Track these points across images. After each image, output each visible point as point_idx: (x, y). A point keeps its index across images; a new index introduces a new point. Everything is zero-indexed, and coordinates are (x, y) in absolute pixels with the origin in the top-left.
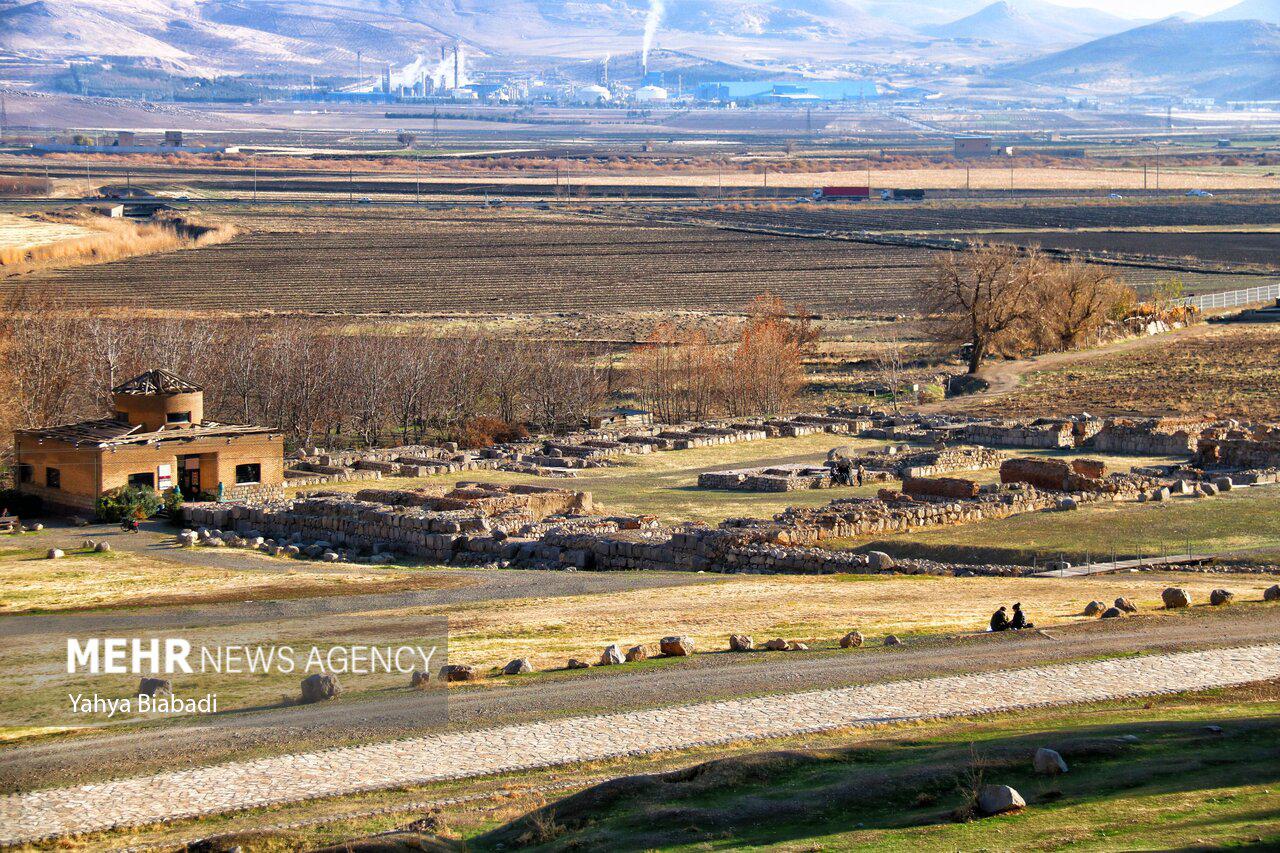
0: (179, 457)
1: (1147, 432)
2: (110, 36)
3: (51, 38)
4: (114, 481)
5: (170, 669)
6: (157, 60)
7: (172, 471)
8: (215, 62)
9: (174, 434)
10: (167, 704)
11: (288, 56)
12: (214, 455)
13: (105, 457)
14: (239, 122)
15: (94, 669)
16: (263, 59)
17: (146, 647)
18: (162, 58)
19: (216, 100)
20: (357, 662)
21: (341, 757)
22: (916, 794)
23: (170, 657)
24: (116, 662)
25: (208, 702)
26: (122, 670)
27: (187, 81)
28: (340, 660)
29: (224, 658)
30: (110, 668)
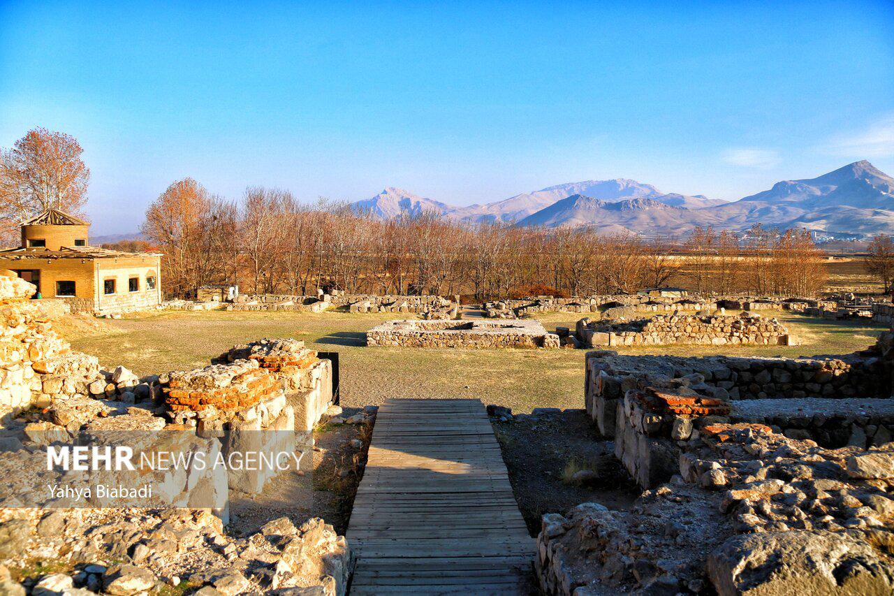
5: (118, 468)
10: (116, 492)
20: (162, 462)
21: (867, 402)
22: (824, 515)
28: (237, 461)
29: (156, 460)
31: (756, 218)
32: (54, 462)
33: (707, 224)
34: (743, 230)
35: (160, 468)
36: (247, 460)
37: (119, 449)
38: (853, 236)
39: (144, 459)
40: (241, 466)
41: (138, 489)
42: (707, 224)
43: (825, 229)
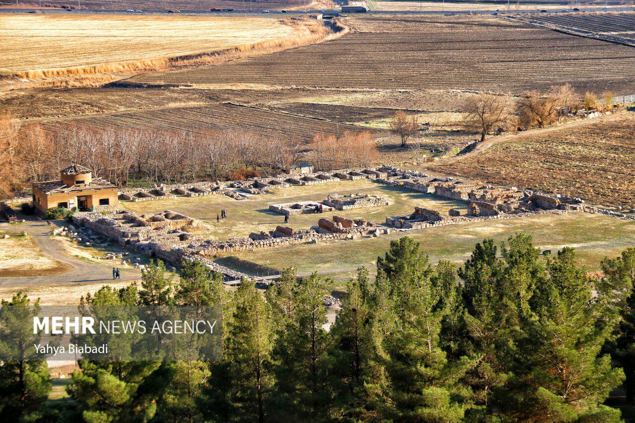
0: (78, 197)
1: (451, 191)
4: (52, 205)
5: (84, 332)
7: (75, 201)
9: (78, 188)
10: (83, 349)
12: (90, 196)
13: (48, 197)
15: (47, 332)
17: (72, 320)
24: (178, 330)
25: (103, 348)
26: (61, 332)
32: (38, 328)
35: (113, 332)
36: (176, 327)
37: (85, 319)
39: (132, 327)
40: (171, 331)
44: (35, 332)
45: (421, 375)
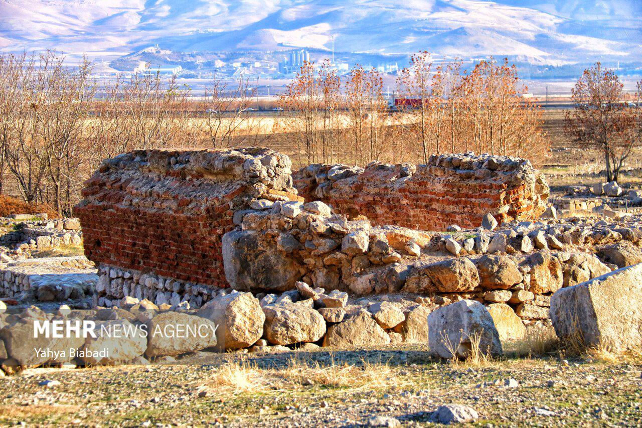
2: (501, 45)
3: (467, 48)
5: (85, 336)
6: (525, 57)
8: (562, 57)
11: (607, 51)
14: (562, 88)
15: (47, 336)
16: (592, 54)
17: (73, 324)
18: (528, 55)
19: (555, 77)
23: (86, 330)
24: (59, 332)
26: (61, 336)
27: (540, 67)
29: (112, 331)
30: (55, 335)
31: (163, 19)
33: (43, 36)
34: (137, 49)
35: (115, 336)
36: (178, 330)
37: (86, 323)
38: (392, 60)
39: (189, 331)
40: (173, 335)
41: (99, 352)
42: (43, 36)
43: (328, 45)
44: (36, 336)
45: (269, 137)
